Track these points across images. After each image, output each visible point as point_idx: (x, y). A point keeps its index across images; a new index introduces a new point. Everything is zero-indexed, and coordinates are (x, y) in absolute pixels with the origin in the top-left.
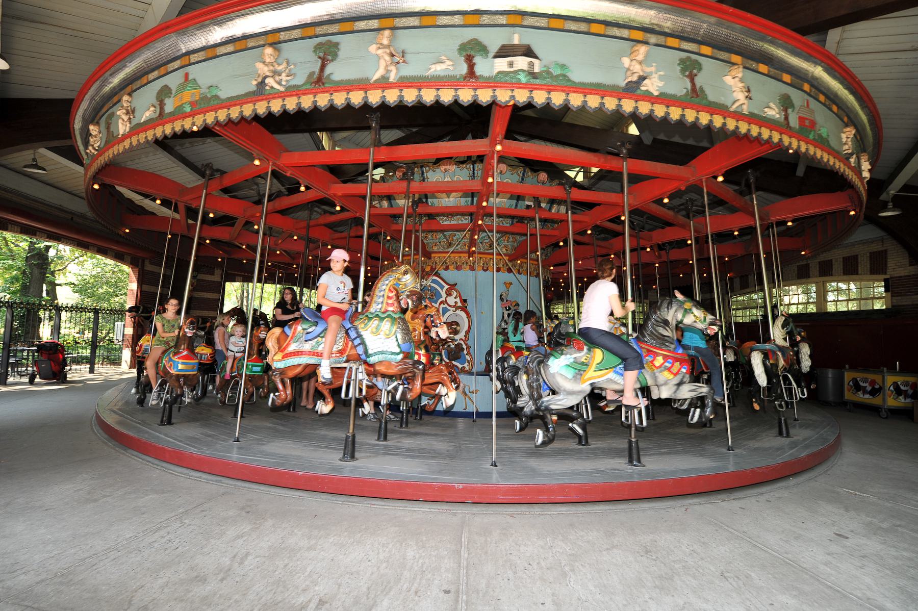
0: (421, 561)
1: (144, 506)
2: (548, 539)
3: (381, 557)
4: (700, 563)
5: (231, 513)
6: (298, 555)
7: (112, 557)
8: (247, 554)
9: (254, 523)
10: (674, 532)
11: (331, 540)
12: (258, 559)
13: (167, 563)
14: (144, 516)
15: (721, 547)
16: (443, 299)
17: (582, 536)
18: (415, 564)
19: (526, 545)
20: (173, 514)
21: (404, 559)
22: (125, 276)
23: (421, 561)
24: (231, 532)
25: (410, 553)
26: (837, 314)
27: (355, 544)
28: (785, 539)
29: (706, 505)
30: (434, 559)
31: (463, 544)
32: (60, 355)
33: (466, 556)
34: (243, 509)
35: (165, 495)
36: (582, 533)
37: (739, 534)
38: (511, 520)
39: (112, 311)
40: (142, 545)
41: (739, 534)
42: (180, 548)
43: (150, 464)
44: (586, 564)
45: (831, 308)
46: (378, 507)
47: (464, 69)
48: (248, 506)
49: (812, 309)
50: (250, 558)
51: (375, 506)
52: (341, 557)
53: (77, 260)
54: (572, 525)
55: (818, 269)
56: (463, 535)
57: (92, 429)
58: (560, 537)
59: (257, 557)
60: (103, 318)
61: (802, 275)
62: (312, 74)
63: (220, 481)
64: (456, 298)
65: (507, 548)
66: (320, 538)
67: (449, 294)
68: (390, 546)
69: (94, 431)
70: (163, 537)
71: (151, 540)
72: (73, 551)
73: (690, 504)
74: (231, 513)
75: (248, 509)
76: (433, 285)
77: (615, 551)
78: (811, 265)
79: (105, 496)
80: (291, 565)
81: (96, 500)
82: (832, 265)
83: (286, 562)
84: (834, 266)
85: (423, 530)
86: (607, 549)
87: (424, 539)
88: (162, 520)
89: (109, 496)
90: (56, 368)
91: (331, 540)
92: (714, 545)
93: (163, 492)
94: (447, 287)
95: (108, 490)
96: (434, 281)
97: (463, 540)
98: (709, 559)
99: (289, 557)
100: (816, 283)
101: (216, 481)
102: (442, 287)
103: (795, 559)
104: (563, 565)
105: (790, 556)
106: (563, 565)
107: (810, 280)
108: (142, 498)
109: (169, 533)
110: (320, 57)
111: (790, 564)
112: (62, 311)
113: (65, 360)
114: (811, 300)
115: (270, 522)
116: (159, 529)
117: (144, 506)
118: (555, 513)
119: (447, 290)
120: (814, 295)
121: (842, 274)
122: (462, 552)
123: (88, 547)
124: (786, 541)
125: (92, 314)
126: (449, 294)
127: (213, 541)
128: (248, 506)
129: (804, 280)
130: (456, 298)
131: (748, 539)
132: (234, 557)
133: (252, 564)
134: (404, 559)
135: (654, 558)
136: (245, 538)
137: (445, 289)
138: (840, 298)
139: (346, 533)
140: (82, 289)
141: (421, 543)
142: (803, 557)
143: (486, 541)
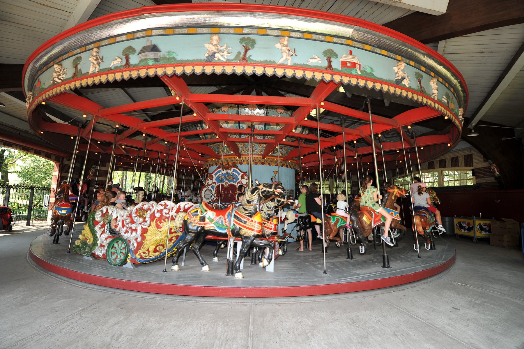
0: (226, 334)
1: (57, 307)
2: (299, 318)
3: (202, 332)
4: (382, 327)
5: (111, 310)
6: (152, 333)
7: (36, 340)
8: (121, 334)
9: (126, 315)
10: (368, 310)
11: (172, 324)
12: (128, 337)
13: (71, 341)
14: (57, 313)
15: (393, 318)
16: (239, 181)
17: (318, 315)
18: (222, 335)
19: (286, 321)
20: (76, 311)
21: (216, 333)
22: (51, 168)
23: (226, 334)
24: (111, 321)
25: (219, 329)
26: (449, 188)
27: (187, 325)
28: (427, 312)
29: (385, 294)
30: (233, 332)
31: (250, 322)
32: (9, 215)
33: (252, 329)
34: (119, 306)
35: (71, 299)
36: (318, 313)
37: (403, 310)
38: (278, 307)
39: (43, 188)
40: (55, 331)
41: (403, 310)
42: (79, 332)
43: (62, 281)
44: (320, 331)
45: (446, 184)
46: (201, 302)
47: (326, 64)
48: (123, 305)
49: (436, 185)
50: (122, 336)
51: (199, 302)
52: (178, 333)
53: (22, 158)
54: (312, 309)
55: (438, 164)
56: (250, 317)
57: (27, 260)
58: (306, 316)
59: (127, 336)
60: (37, 192)
61: (430, 167)
62: (239, 53)
63: (106, 290)
64: (246, 180)
65: (276, 324)
66: (166, 323)
67: (243, 178)
68: (208, 326)
69: (27, 261)
70: (69, 326)
71: (61, 328)
72: (10, 337)
73: (376, 294)
74: (111, 310)
75: (122, 306)
76: (233, 172)
77: (336, 323)
78: (435, 162)
79: (33, 301)
80: (148, 340)
81: (27, 304)
82: (445, 161)
83: (145, 338)
84: (446, 163)
85: (227, 315)
86: (332, 322)
87: (228, 320)
88: (69, 315)
89: (35, 301)
90: (5, 223)
91: (172, 324)
92: (390, 317)
93: (70, 298)
94: (241, 174)
95: (35, 297)
96: (234, 171)
97: (250, 320)
98: (387, 325)
99: (147, 335)
100: (438, 171)
101: (103, 290)
102: (239, 174)
103: (433, 323)
104: (307, 332)
105: (429, 321)
106: (307, 332)
107: (435, 170)
108: (57, 302)
109: (72, 323)
110: (244, 46)
111: (430, 326)
112: (11, 188)
113: (11, 218)
114: (436, 181)
115: (136, 314)
116: (67, 321)
117: (57, 307)
118: (302, 302)
119: (242, 175)
120: (437, 178)
121: (464, 166)
122: (250, 328)
123: (20, 334)
124: (428, 313)
125: (30, 190)
126: (243, 178)
127: (100, 327)
128: (123, 305)
129: (432, 170)
130: (246, 180)
131: (408, 313)
132: (113, 336)
133: (124, 340)
134: (216, 333)
135: (357, 326)
136: (119, 325)
137: (240, 175)
138: (450, 179)
139: (181, 319)
140: (23, 175)
141: (225, 323)
142: (437, 322)
143: (263, 320)
